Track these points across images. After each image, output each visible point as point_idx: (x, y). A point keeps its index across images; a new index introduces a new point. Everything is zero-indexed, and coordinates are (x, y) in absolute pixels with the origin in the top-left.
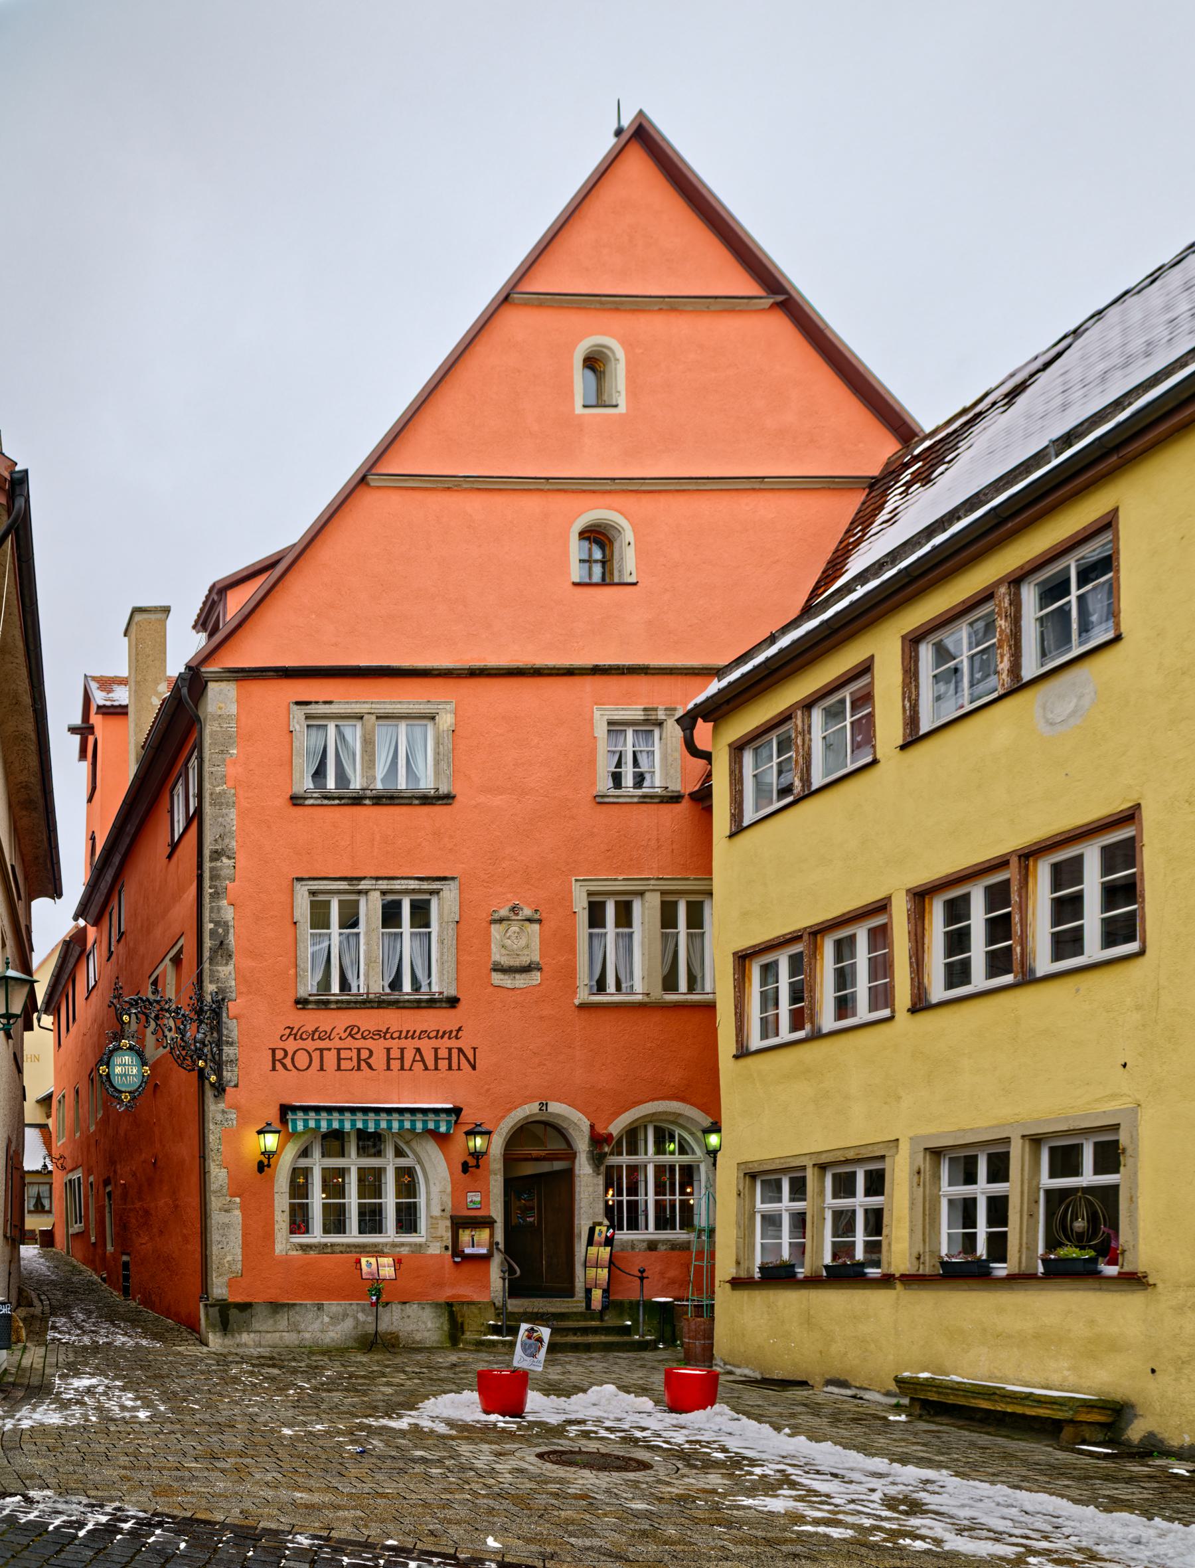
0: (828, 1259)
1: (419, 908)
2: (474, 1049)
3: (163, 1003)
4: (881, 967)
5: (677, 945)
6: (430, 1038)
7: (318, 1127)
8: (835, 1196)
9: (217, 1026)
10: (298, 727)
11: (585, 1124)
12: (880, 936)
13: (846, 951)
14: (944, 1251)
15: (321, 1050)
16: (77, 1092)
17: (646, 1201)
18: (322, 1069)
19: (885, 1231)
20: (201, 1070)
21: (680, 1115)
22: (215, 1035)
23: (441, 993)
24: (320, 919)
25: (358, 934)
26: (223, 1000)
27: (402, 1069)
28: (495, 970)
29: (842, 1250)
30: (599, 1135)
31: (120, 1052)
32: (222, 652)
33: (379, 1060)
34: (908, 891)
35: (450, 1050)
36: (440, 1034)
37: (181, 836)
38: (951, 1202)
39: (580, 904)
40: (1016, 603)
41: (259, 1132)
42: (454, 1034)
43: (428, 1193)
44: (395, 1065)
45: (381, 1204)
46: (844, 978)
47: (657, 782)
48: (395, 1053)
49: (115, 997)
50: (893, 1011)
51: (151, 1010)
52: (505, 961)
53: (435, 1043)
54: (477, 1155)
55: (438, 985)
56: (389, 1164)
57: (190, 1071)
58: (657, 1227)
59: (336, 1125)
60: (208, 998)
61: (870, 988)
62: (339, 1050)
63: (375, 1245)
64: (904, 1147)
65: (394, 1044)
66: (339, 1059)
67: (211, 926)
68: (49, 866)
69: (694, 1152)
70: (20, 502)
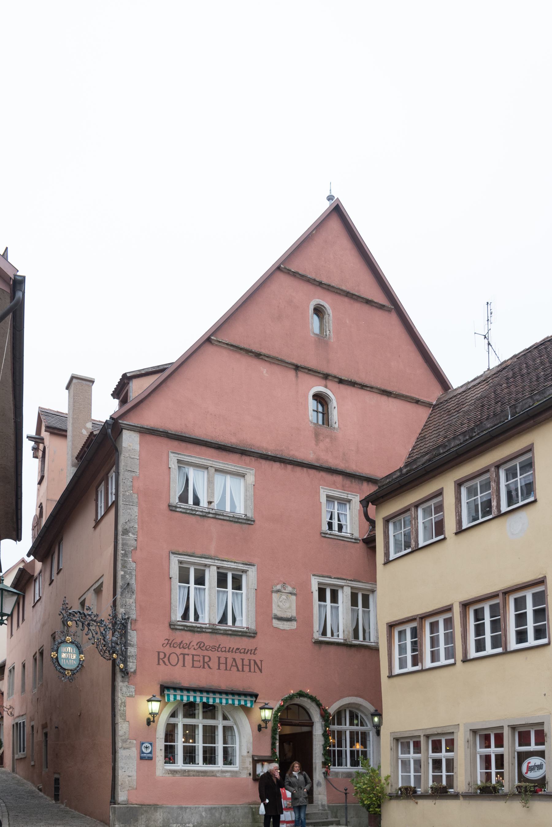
0: (431, 783)
1: (236, 579)
2: (261, 661)
3: (93, 616)
4: (450, 638)
5: (358, 616)
6: (241, 653)
7: (182, 700)
8: (433, 752)
9: (124, 635)
10: (173, 466)
12: (449, 623)
13: (435, 628)
14: (479, 783)
16: (24, 666)
17: (346, 751)
18: (184, 666)
19: (455, 770)
20: (114, 661)
21: (361, 705)
22: (123, 639)
23: (247, 628)
25: (204, 589)
26: (128, 618)
27: (226, 669)
28: (275, 618)
29: (438, 779)
32: (131, 414)
33: (214, 664)
34: (460, 603)
35: (250, 660)
36: (246, 651)
37: (103, 517)
38: (481, 756)
39: (315, 588)
40: (498, 476)
41: (148, 701)
42: (253, 651)
43: (240, 742)
44: (223, 666)
45: (215, 747)
46: (434, 642)
47: (348, 531)
48: (223, 660)
49: (63, 609)
50: (455, 661)
51: (85, 618)
52: (280, 614)
53: (242, 656)
56: (220, 723)
57: (108, 660)
58: (351, 765)
59: (192, 699)
60: (120, 616)
61: (445, 648)
62: (193, 655)
63: (212, 772)
64: (462, 728)
65: (223, 655)
66: (193, 661)
67: (122, 573)
68: (15, 520)
69: (367, 726)
70: (19, 294)
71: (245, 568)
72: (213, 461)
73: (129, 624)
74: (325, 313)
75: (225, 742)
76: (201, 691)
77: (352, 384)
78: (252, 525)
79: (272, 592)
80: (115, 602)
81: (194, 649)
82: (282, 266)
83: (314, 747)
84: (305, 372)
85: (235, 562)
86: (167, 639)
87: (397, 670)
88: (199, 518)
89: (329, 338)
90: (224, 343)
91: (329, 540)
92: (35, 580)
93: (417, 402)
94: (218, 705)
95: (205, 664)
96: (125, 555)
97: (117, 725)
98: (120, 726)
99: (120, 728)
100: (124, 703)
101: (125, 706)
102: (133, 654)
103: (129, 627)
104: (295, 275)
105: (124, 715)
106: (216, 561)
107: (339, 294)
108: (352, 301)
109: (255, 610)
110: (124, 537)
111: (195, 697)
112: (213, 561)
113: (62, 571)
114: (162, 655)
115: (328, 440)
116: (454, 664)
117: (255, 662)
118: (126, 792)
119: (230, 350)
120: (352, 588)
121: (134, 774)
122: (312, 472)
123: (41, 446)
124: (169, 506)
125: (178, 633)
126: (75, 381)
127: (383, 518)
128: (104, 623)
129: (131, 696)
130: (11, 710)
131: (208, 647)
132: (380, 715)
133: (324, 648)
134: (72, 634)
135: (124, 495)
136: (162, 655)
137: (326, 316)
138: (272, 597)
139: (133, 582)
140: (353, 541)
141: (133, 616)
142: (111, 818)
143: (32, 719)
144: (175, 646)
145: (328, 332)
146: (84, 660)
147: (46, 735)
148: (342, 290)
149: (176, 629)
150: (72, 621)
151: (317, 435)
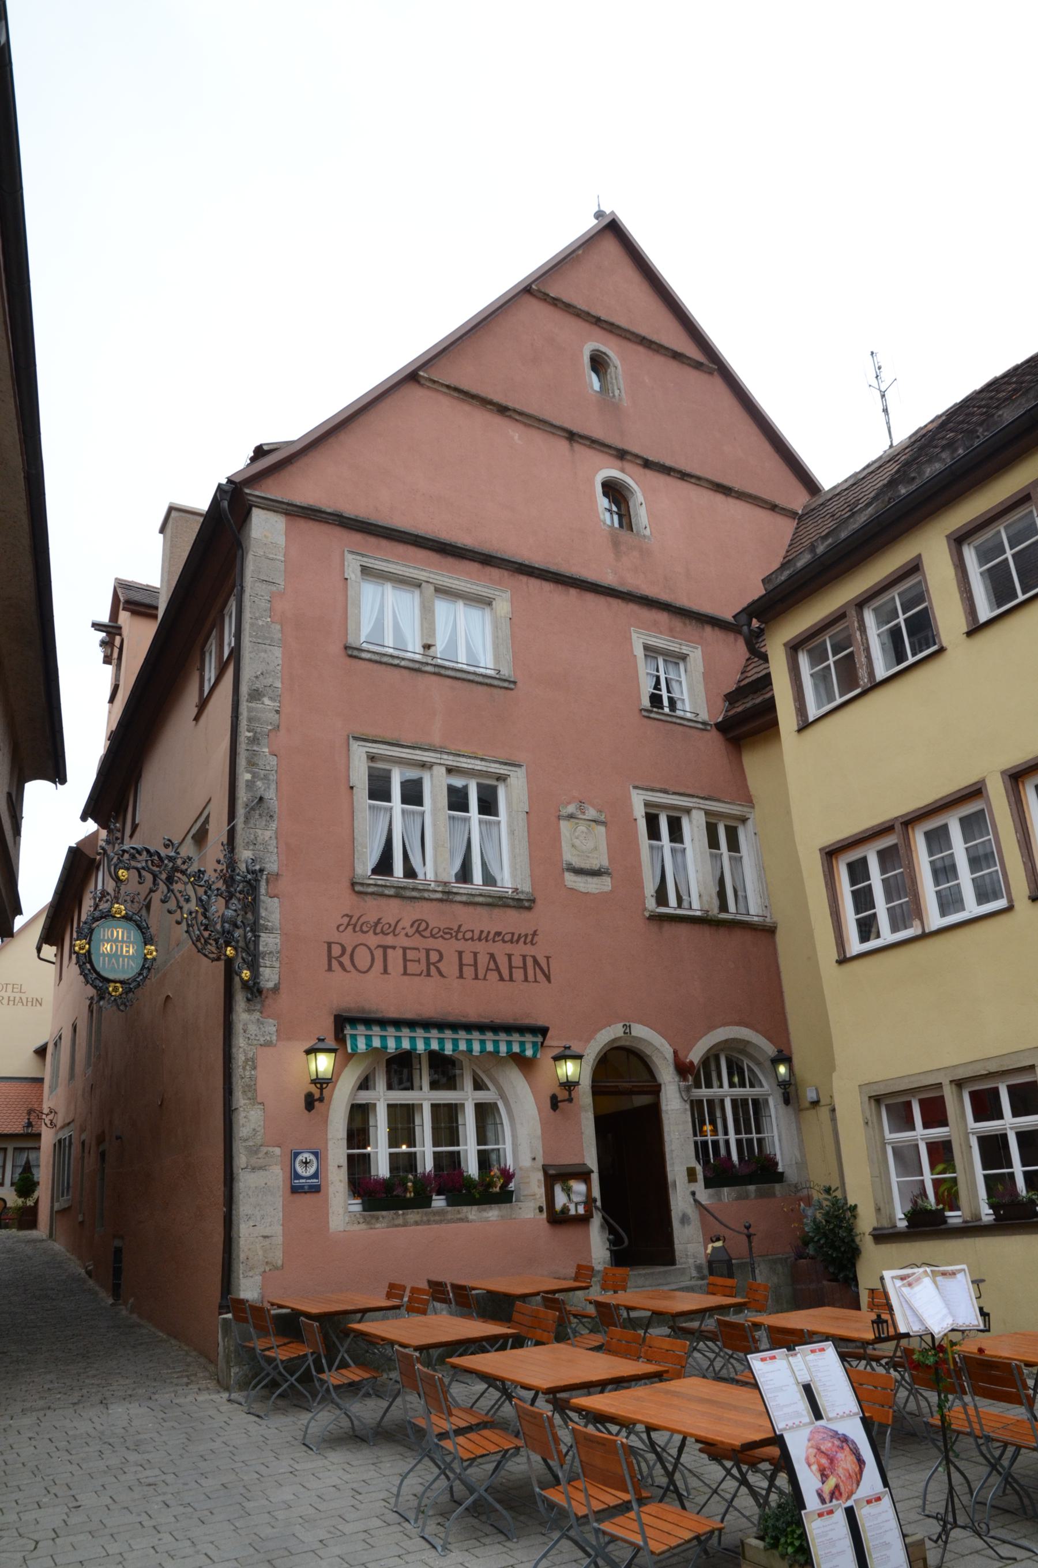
2: (548, 958)
6: (504, 942)
8: (977, 1119)
9: (252, 905)
10: (353, 577)
11: (668, 1052)
15: (385, 948)
18: (385, 971)
20: (229, 962)
21: (748, 1042)
22: (249, 916)
24: (379, 791)
26: (261, 870)
27: (476, 978)
30: (684, 1064)
31: (110, 922)
33: (449, 966)
34: (1003, 773)
35: (524, 957)
36: (516, 937)
39: (639, 812)
44: (468, 971)
46: (944, 871)
48: (468, 959)
50: (1010, 900)
52: (577, 862)
53: (509, 948)
54: (569, 1085)
55: (507, 880)
59: (406, 1045)
60: (243, 867)
62: (405, 949)
65: (468, 947)
66: (405, 960)
67: (248, 776)
69: (762, 1086)
71: (502, 772)
72: (430, 572)
73: (263, 883)
74: (609, 365)
75: (481, 1139)
76: (427, 1025)
77: (666, 470)
78: (511, 689)
79: (559, 818)
80: (232, 834)
81: (407, 935)
82: (534, 286)
83: (667, 1138)
84: (585, 445)
85: (482, 759)
86: (347, 915)
87: (855, 946)
88: (405, 672)
89: (620, 399)
90: (442, 385)
91: (656, 722)
92: (98, 869)
93: (773, 507)
94: (461, 1058)
95: (432, 967)
96: (254, 740)
97: (235, 1114)
98: (243, 1114)
99: (242, 1121)
100: (253, 1060)
101: (254, 1068)
102: (272, 947)
103: (263, 891)
104: (556, 302)
105: (251, 1089)
106: (445, 757)
107: (629, 339)
108: (650, 353)
109: (527, 853)
110: (253, 705)
111: (413, 1039)
112: (439, 756)
113: (138, 829)
114: (336, 951)
115: (636, 553)
116: (1010, 908)
117: (536, 961)
118: (259, 1278)
119: (454, 397)
120: (708, 813)
121: (277, 1230)
122: (615, 603)
123: (118, 639)
124: (346, 648)
125: (371, 903)
126: (174, 514)
127: (785, 645)
128: (206, 878)
129: (268, 1044)
130: (51, 1117)
131: (435, 931)
132: (788, 1060)
133: (669, 928)
134: (128, 898)
135: (252, 625)
136: (336, 951)
137: (611, 370)
138: (559, 829)
139: (270, 794)
140: (700, 726)
141: (272, 865)
142: (221, 1349)
143: (82, 1130)
144: (365, 929)
145: (617, 392)
146: (154, 959)
147: (103, 1155)
148: (633, 333)
149: (366, 893)
150: (127, 869)
151: (616, 544)
